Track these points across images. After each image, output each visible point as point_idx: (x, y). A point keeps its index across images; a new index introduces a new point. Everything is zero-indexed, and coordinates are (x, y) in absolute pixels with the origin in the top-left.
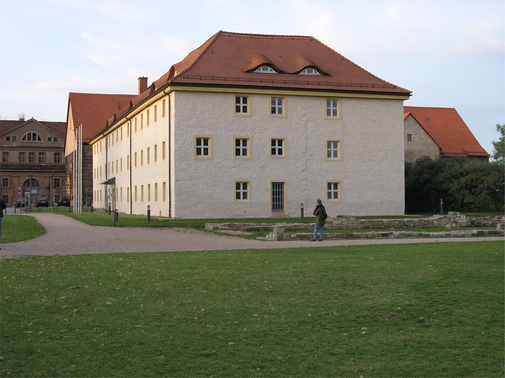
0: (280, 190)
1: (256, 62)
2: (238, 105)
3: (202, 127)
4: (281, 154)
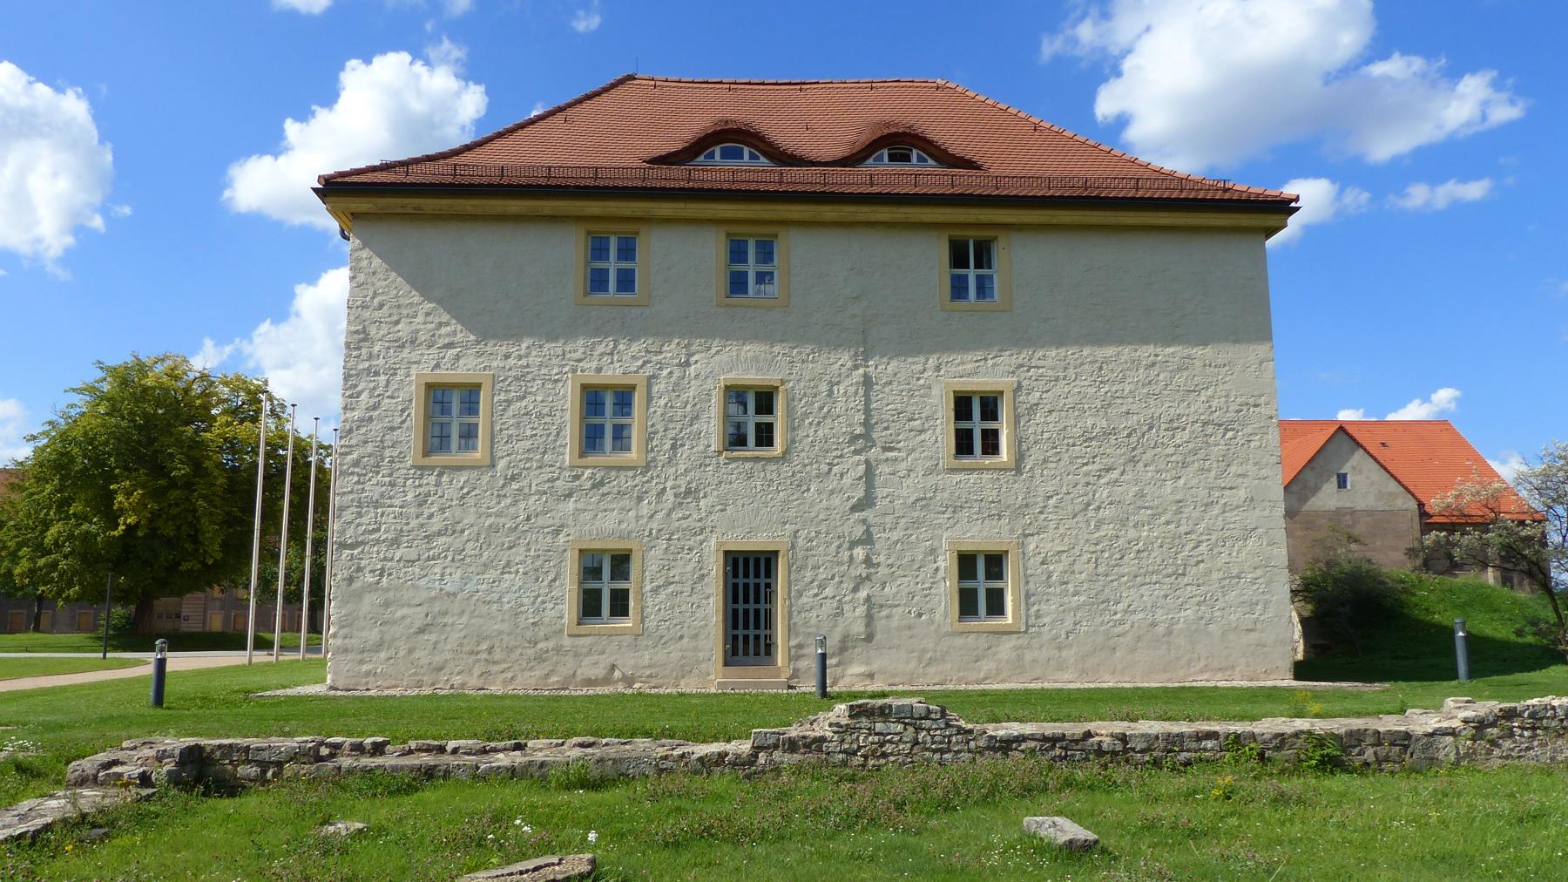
3: (450, 345)
4: (770, 443)
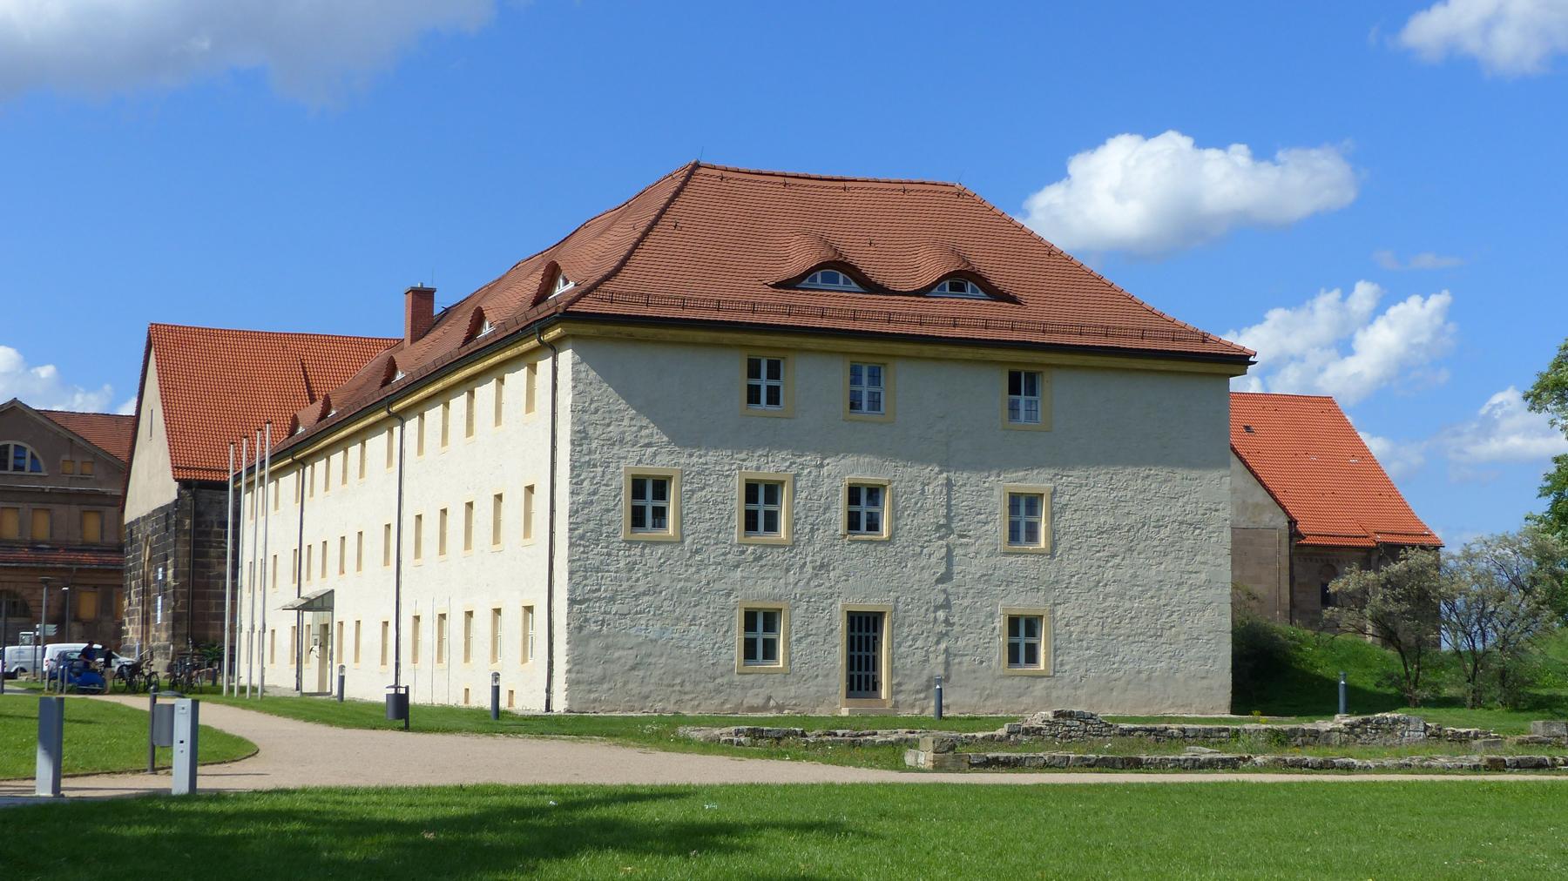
0: (871, 634)
1: (800, 258)
2: (754, 382)
3: (649, 445)
